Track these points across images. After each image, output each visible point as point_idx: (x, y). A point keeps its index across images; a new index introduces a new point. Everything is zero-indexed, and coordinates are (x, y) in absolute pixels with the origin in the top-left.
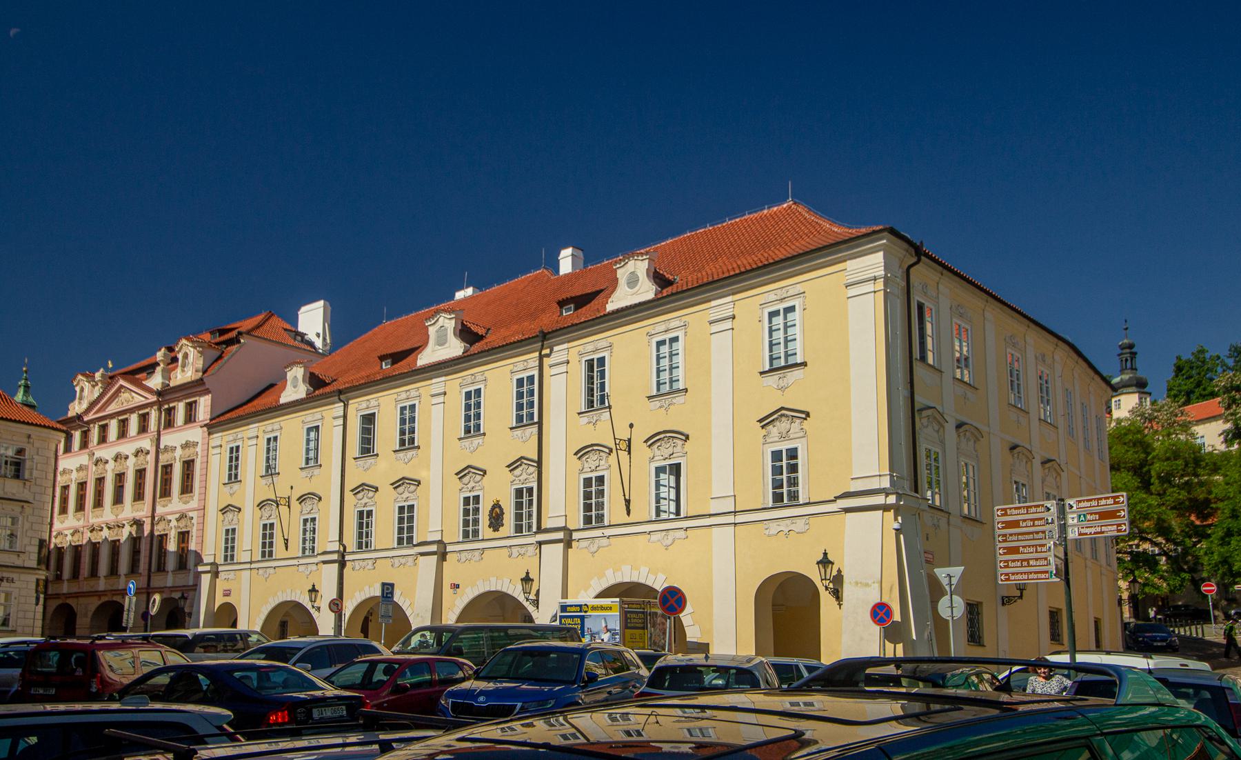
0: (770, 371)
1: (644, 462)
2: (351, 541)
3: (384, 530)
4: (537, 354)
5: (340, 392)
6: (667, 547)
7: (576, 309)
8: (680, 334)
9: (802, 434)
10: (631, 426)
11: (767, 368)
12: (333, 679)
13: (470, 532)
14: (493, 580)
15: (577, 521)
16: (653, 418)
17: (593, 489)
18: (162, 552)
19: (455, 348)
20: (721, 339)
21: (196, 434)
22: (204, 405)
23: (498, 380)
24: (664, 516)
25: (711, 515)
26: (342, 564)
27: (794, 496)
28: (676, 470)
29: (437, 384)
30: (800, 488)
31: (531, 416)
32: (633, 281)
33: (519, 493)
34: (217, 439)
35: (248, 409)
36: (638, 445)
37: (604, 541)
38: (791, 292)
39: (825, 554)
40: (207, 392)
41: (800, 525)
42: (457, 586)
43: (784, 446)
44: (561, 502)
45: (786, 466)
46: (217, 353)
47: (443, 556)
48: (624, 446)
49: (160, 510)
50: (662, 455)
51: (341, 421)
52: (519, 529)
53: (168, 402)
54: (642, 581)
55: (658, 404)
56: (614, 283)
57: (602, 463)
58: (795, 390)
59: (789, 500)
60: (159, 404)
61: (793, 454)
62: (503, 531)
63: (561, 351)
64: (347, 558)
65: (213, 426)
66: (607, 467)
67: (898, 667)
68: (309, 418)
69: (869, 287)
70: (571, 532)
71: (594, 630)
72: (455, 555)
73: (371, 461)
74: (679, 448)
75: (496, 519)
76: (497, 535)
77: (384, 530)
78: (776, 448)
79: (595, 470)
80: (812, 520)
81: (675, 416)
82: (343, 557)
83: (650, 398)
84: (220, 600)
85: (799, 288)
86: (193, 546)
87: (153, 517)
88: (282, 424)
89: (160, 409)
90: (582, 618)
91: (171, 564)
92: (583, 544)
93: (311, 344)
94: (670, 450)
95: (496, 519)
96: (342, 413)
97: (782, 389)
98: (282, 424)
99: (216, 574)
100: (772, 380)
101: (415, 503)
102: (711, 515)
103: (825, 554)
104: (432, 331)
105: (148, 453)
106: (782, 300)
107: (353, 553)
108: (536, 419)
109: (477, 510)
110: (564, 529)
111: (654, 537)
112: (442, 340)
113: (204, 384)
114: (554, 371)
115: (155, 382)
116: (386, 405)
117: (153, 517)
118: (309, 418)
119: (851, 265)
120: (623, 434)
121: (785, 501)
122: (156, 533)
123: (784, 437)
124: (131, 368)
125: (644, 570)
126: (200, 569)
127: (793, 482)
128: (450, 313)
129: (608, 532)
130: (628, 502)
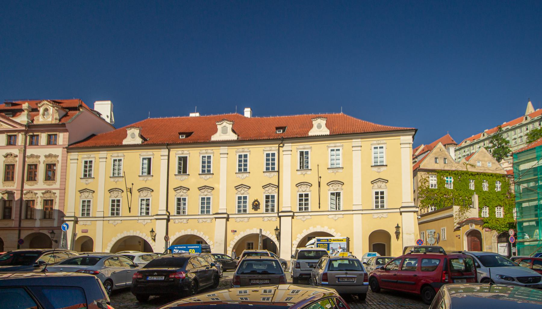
1: (136, 197)
2: (173, 210)
4: (277, 145)
5: (168, 145)
6: (304, 221)
7: (186, 137)
8: (122, 158)
10: (133, 184)
12: (360, 269)
13: (242, 210)
14: (196, 231)
17: (304, 199)
18: (33, 210)
19: (139, 141)
22: (62, 138)
23: (257, 154)
24: (142, 214)
25: (353, 210)
26: (168, 220)
28: (338, 194)
29: (224, 149)
30: (385, 204)
31: (273, 169)
32: (224, 131)
33: (267, 197)
34: (74, 155)
35: (82, 145)
36: (135, 191)
37: (309, 217)
40: (66, 131)
41: (385, 215)
42: (236, 231)
45: (380, 196)
46: (64, 113)
47: (227, 219)
48: (129, 190)
49: (27, 187)
50: (334, 189)
51: (167, 158)
52: (267, 210)
53: (33, 132)
56: (311, 126)
57: (308, 189)
60: (26, 132)
61: (382, 193)
62: (259, 211)
63: (288, 146)
64: (170, 218)
65: (71, 147)
66: (123, 198)
68: (144, 154)
69: (408, 146)
71: (334, 248)
73: (185, 177)
74: (149, 194)
76: (256, 212)
78: (377, 191)
79: (146, 197)
80: (389, 214)
82: (169, 217)
83: (328, 169)
84: (79, 234)
85: (385, 142)
86: (56, 207)
87: (22, 191)
88: (125, 154)
89: (25, 134)
90: (328, 244)
91: (38, 216)
92: (298, 217)
93: (104, 120)
94: (337, 187)
96: (167, 154)
97: (379, 172)
98: (125, 154)
99: (76, 222)
100: (376, 169)
102: (353, 210)
104: (219, 127)
105: (16, 156)
106: (379, 144)
108: (276, 169)
110: (74, 217)
111: (330, 216)
112: (224, 131)
113: (65, 126)
115: (23, 119)
116: (195, 155)
117: (22, 191)
118: (144, 154)
119: (402, 138)
120: (129, 186)
122: (24, 199)
123: (380, 187)
124: (56, 100)
125: (132, 231)
127: (88, 210)
128: (230, 121)
130: (130, 208)
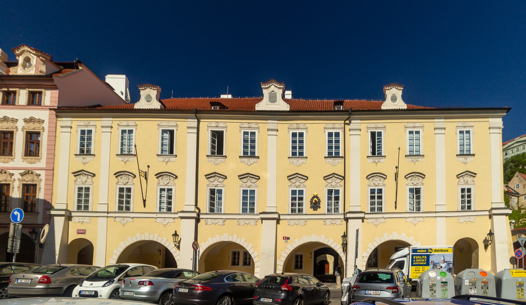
0: (120, 155)
2: (204, 205)
3: (232, 201)
9: (472, 183)
11: (119, 153)
15: (73, 207)
16: (408, 166)
17: (376, 195)
20: (440, 136)
21: (43, 114)
24: (162, 210)
25: (96, 212)
26: (198, 220)
27: (87, 207)
36: (151, 176)
37: (383, 220)
38: (468, 125)
39: (176, 232)
42: (288, 238)
43: (466, 187)
44: (357, 197)
45: (466, 195)
48: (143, 174)
51: (195, 131)
54: (155, 240)
55: (410, 160)
58: (471, 164)
59: (468, 209)
62: (319, 211)
63: (355, 123)
64: (201, 216)
65: (61, 110)
66: (135, 185)
67: (23, 276)
68: (164, 123)
70: (70, 212)
72: (204, 220)
75: (315, 205)
76: (315, 212)
77: (232, 201)
78: (463, 187)
81: (418, 166)
85: (472, 124)
86: (41, 195)
90: (428, 256)
95: (315, 205)
96: (196, 126)
99: (69, 218)
100: (462, 159)
101: (304, 189)
102: (96, 212)
103: (176, 232)
106: (465, 127)
107: (206, 214)
109: (301, 199)
114: (352, 132)
118: (164, 123)
119: (491, 120)
120: (144, 169)
121: (83, 209)
123: (467, 183)
125: (156, 235)
126: (53, 212)
127: (87, 201)
129: (385, 216)
130: (144, 201)
